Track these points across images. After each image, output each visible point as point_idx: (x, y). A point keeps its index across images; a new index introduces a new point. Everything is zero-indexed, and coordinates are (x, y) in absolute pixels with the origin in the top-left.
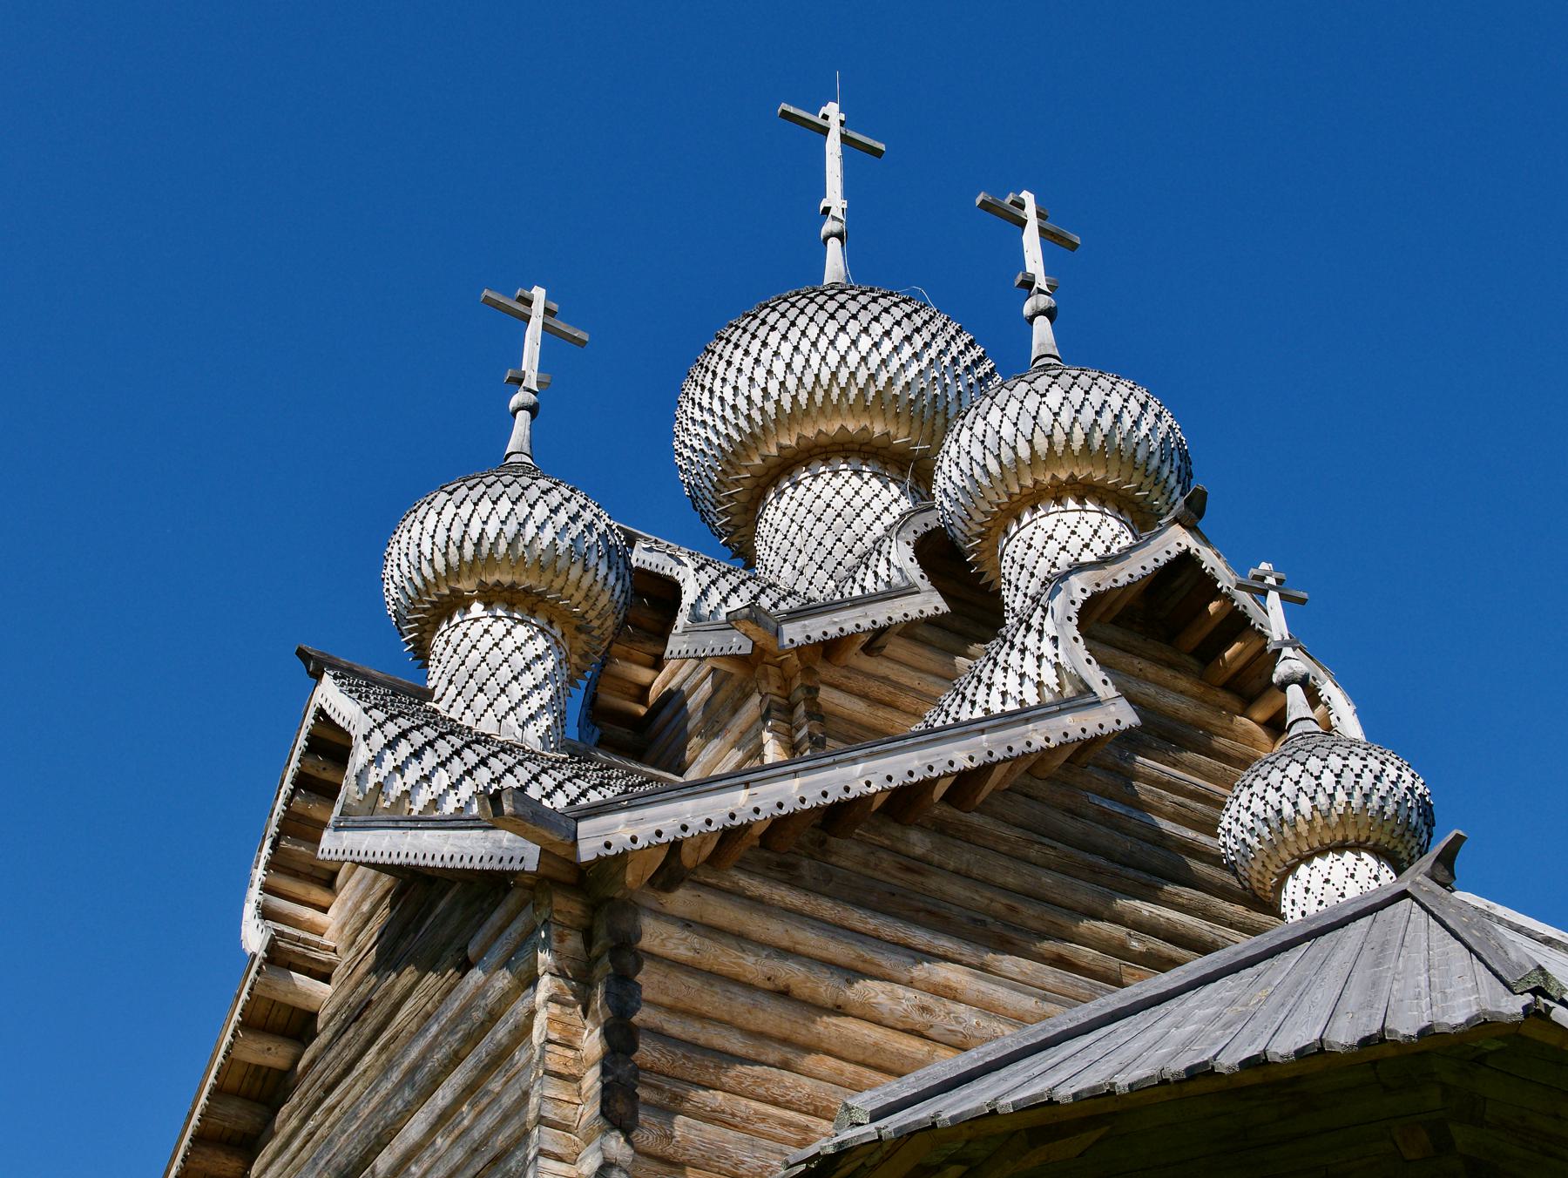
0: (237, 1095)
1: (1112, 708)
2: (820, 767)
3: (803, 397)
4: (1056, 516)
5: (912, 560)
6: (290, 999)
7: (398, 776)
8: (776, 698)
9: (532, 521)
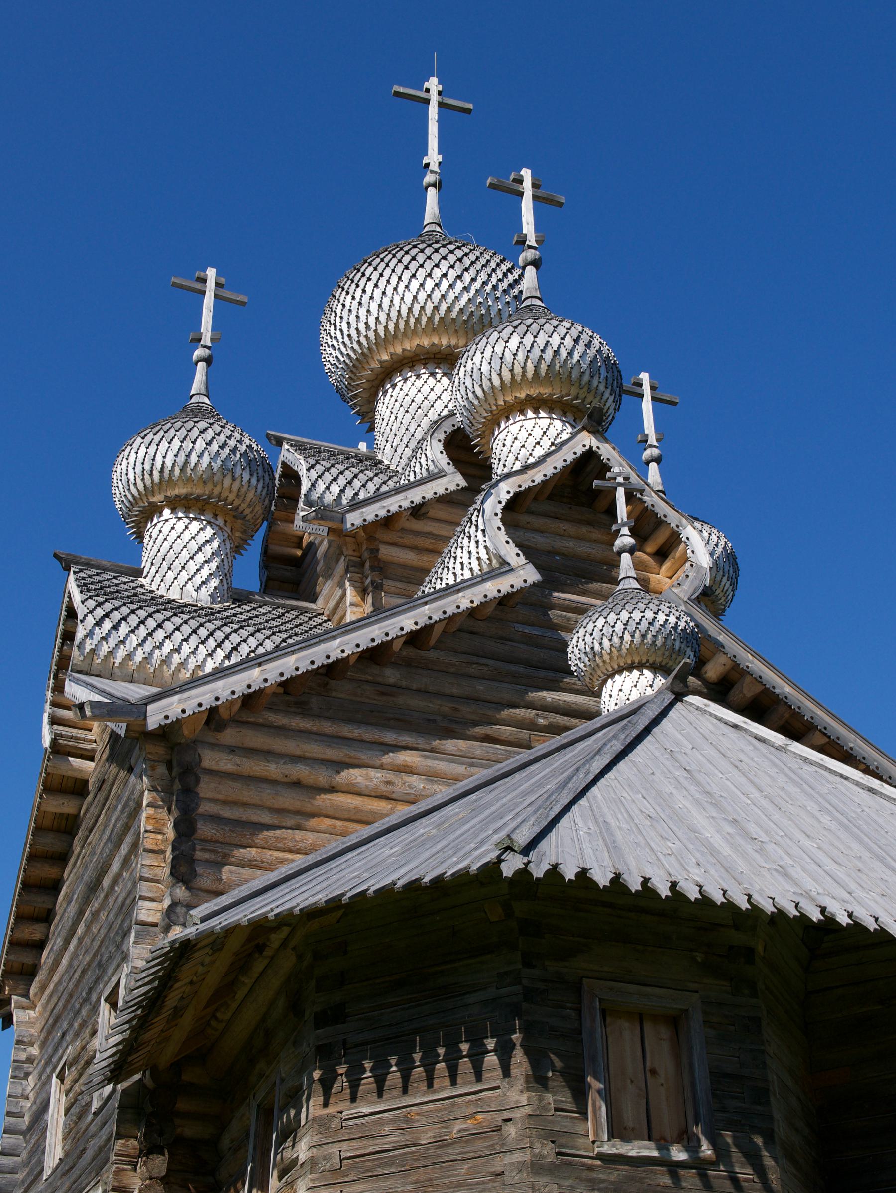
0: (52, 830)
1: (522, 572)
2: (310, 645)
3: (391, 327)
4: (520, 423)
5: (442, 453)
6: (70, 774)
7: (104, 642)
8: (353, 558)
9: (194, 452)
